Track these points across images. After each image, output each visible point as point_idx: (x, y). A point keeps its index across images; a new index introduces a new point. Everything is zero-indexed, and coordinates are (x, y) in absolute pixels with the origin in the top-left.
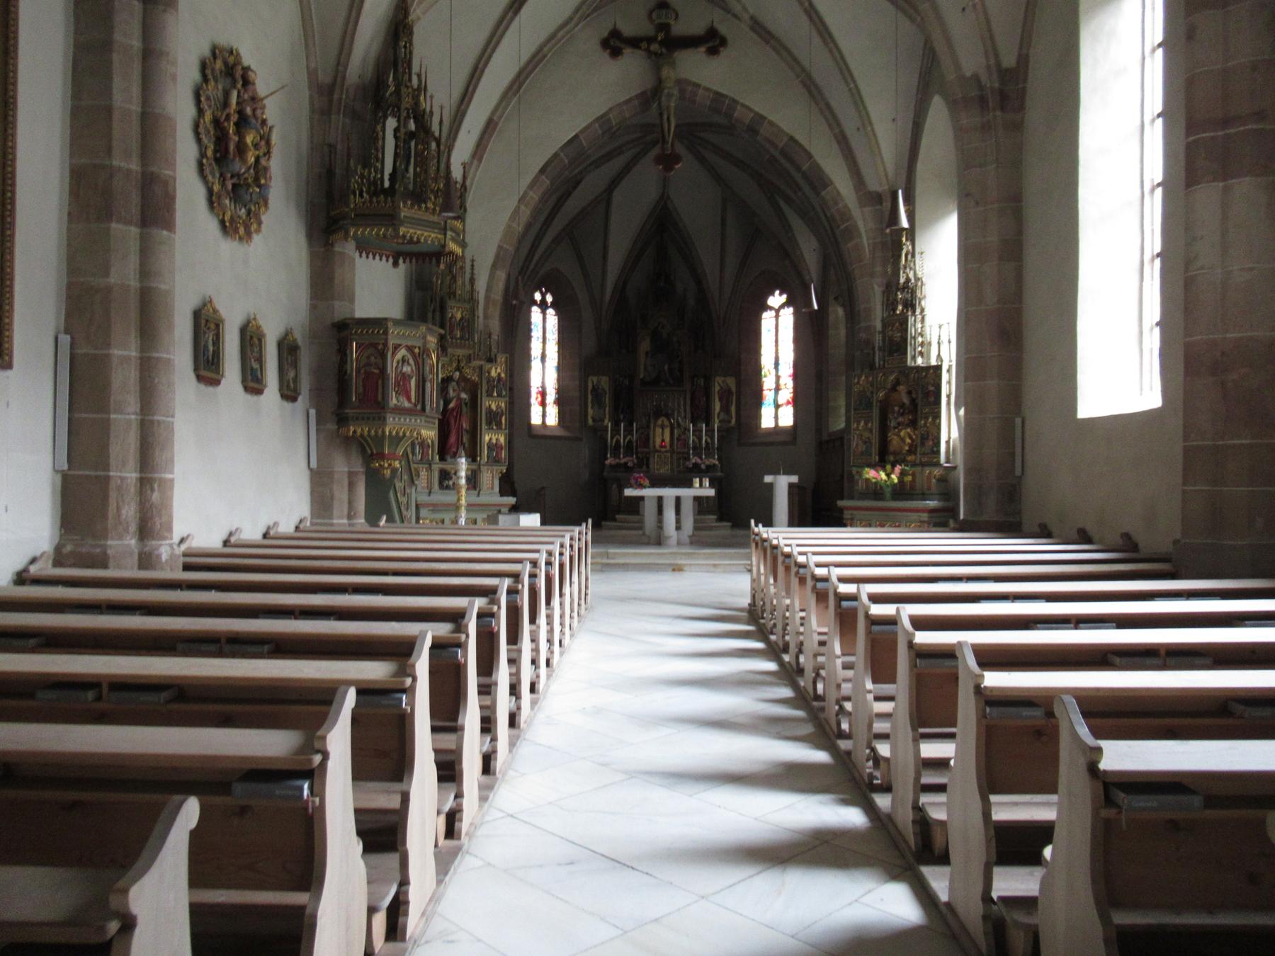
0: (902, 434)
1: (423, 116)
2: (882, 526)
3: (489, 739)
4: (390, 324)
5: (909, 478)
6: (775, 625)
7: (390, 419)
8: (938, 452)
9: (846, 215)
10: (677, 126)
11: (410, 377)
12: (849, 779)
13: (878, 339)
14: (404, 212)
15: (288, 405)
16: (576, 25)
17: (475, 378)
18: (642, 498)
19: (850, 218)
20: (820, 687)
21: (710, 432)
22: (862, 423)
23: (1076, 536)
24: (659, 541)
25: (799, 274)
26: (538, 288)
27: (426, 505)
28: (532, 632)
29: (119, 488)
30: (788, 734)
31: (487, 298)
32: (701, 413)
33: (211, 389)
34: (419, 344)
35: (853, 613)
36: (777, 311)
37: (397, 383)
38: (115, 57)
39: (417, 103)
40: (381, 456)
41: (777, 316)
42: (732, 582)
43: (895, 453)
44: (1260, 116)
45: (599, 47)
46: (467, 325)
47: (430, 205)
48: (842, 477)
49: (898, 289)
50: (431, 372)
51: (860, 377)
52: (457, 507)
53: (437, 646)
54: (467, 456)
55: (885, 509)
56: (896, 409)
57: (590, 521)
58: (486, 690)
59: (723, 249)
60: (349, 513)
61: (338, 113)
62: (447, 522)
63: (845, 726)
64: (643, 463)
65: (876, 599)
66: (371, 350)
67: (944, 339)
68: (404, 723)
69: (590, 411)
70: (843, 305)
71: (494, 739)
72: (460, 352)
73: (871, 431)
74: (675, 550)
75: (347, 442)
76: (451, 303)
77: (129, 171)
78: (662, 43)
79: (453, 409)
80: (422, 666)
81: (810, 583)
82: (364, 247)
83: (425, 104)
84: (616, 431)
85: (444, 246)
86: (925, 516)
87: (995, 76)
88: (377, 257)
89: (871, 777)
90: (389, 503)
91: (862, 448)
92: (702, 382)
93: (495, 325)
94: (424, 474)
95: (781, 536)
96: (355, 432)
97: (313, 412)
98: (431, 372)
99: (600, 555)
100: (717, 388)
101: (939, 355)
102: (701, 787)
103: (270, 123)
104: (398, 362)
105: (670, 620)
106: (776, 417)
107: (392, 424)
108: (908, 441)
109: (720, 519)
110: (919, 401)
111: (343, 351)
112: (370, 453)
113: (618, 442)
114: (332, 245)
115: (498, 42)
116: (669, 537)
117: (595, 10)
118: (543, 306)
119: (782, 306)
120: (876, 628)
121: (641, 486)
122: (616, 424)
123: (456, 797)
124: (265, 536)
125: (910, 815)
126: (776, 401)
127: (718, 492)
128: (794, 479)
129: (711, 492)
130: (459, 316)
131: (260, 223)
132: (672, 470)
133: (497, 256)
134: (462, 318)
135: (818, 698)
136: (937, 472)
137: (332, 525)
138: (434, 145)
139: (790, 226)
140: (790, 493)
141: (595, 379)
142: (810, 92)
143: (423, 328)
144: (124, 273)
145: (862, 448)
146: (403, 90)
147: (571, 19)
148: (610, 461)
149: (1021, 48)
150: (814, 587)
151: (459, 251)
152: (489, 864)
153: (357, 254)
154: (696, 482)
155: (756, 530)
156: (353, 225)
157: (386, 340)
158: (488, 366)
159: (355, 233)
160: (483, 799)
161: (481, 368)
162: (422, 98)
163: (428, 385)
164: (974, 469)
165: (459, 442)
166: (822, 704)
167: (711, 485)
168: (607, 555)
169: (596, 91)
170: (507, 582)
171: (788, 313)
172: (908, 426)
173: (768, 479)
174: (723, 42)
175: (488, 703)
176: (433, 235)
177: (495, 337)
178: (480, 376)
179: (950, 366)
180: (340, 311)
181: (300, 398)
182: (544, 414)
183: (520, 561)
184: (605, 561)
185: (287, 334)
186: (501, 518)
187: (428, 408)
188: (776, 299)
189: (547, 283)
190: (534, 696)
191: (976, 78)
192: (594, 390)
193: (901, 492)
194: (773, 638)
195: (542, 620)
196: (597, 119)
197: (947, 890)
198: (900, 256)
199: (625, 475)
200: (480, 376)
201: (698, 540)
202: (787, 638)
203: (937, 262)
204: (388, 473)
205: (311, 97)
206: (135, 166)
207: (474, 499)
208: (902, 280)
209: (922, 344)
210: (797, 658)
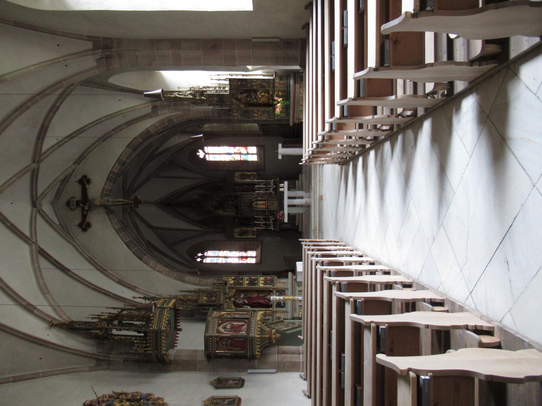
0: (260, 96)
1: (111, 317)
2: (302, 105)
3: (395, 285)
4: (208, 334)
5: (280, 93)
6: (350, 152)
8: (268, 80)
9: (162, 122)
10: (124, 198)
11: (232, 325)
12: (443, 108)
13: (217, 108)
14: (155, 327)
15: (246, 383)
16: (76, 243)
17: (234, 291)
18: (289, 214)
19: (163, 120)
20: (384, 128)
21: (259, 183)
22: (255, 115)
23: (308, 10)
25: (190, 144)
26: (195, 259)
27: (293, 314)
28: (347, 265)
30: (412, 143)
31: (197, 285)
32: (251, 187)
33: (242, 402)
34: (216, 321)
35: (350, 108)
36: (206, 154)
37: (235, 331)
39: (105, 320)
40: (270, 338)
41: (208, 154)
42: (328, 173)
43: (269, 100)
46: (210, 294)
47: (152, 315)
48: (279, 125)
49: (195, 99)
50: (230, 314)
51: (234, 116)
52: (294, 300)
53: (340, 290)
54: (270, 294)
55: (294, 104)
56: (249, 99)
57: (300, 240)
58: (360, 274)
60: (297, 353)
61: (109, 357)
62: (300, 304)
63: (409, 113)
64: (273, 213)
65: (332, 114)
66: (220, 344)
67: (217, 77)
68: (393, 327)
69: (250, 236)
70: (203, 124)
71: (396, 283)
72: (222, 297)
73: (258, 111)
74: (312, 199)
75: (263, 354)
76: (200, 302)
78: (85, 205)
79: (248, 301)
80: (366, 319)
81: (333, 134)
82: (172, 345)
83: (106, 316)
84: (259, 225)
85: (171, 309)
86: (298, 86)
87: (97, 51)
88: (177, 338)
89: (443, 95)
91: (266, 115)
93: (210, 281)
94: (278, 315)
95: (307, 150)
96: (258, 352)
97: (249, 371)
98: (230, 314)
99: (315, 233)
100: (240, 180)
101: (224, 80)
102: (448, 188)
103: (111, 393)
104: (225, 331)
105: (347, 203)
106: (253, 154)
107: (255, 333)
108: (263, 94)
109: (298, 179)
110: (245, 89)
111: (220, 357)
112: (268, 344)
113: (263, 224)
114: (171, 361)
115: (84, 280)
116: (307, 202)
117: (70, 235)
118: (203, 257)
119: (204, 152)
120: (362, 94)
121: (283, 214)
122: (255, 225)
123: (425, 301)
124: (309, 397)
125: (476, 67)
126: (245, 154)
127: (286, 180)
128: (280, 145)
129: (286, 183)
130: (205, 298)
131: (159, 398)
133: (179, 280)
134: (207, 297)
135: (392, 128)
136: (277, 80)
137: (303, 362)
138: (125, 312)
140: (287, 147)
141: (235, 234)
142: (107, 138)
143: (209, 318)
145: (266, 115)
146: (99, 326)
148: (272, 228)
149: (84, 39)
150: (335, 131)
151: (173, 301)
152: (510, 311)
153: (176, 348)
154: (281, 190)
155: (304, 162)
156: (161, 352)
157: (215, 336)
158: (228, 285)
159: (164, 351)
160: (461, 309)
161: (229, 288)
162: (103, 317)
163: (236, 316)
164: (277, 61)
165: (263, 298)
166: (395, 126)
167: (283, 183)
168: (315, 230)
169: (104, 233)
170: (319, 266)
172: (256, 94)
173: (280, 157)
174: (85, 177)
175: (379, 286)
176: (165, 314)
177: (215, 281)
179: (230, 75)
180: (201, 357)
181: (243, 377)
182: (251, 257)
183: (316, 270)
184: (318, 231)
185: (212, 384)
186: (298, 280)
187: (247, 316)
188: (201, 154)
189: (193, 256)
190: (392, 273)
191: (97, 60)
192: (240, 235)
193: (286, 97)
194: (357, 153)
195: (341, 259)
196: (118, 234)
197: (531, 38)
198: (180, 98)
199: (278, 222)
200: (233, 288)
201: (308, 189)
202: (357, 146)
203: (183, 80)
204: (278, 335)
205: (103, 370)
207: (290, 292)
208: (191, 97)
209: (220, 88)
210: (368, 140)
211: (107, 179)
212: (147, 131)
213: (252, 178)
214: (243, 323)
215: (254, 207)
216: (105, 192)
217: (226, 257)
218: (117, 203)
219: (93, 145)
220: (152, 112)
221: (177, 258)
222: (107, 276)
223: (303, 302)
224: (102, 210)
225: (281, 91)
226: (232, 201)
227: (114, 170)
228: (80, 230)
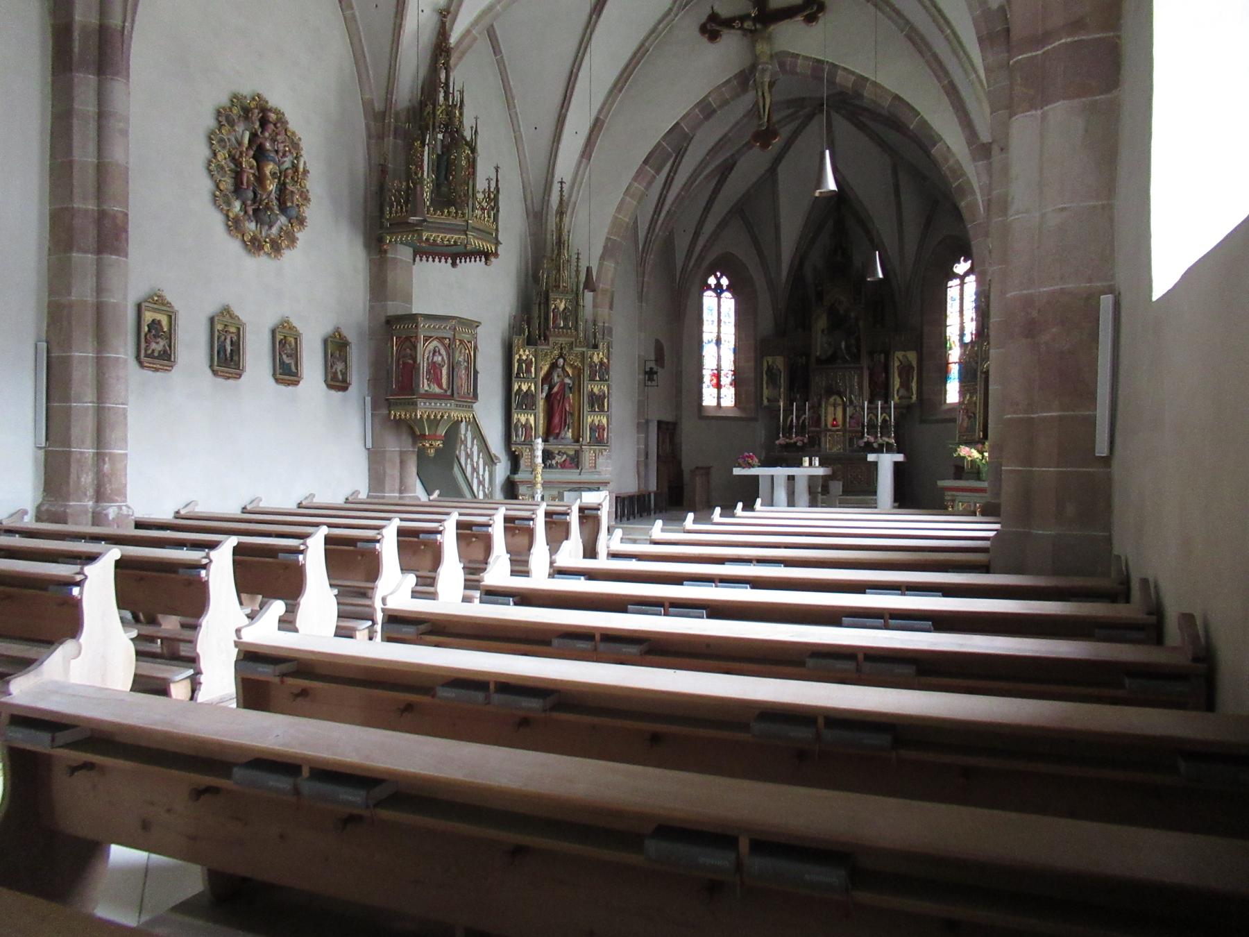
7: (421, 404)
9: (958, 172)
17: (578, 364)
19: (963, 174)
21: (885, 409)
29: (79, 461)
32: (880, 391)
34: (450, 334)
36: (962, 278)
38: (75, 121)
44: (1077, 25)
45: (697, 33)
69: (766, 392)
72: (562, 340)
75: (398, 423)
76: (552, 296)
77: (86, 211)
78: (755, 20)
79: (557, 393)
84: (788, 411)
90: (454, 479)
97: (368, 399)
100: (897, 364)
114: (386, 252)
118: (718, 290)
119: (967, 274)
122: (790, 403)
128: (900, 457)
130: (562, 306)
132: (845, 450)
133: (605, 247)
137: (383, 497)
141: (770, 359)
144: (82, 291)
147: (671, 9)
154: (806, 460)
173: (871, 457)
180: (394, 308)
182: (719, 395)
188: (962, 267)
189: (724, 265)
192: (769, 369)
200: (583, 361)
206: (91, 206)
212: (935, 139)
213: (902, 392)
214: (445, 386)
216: (789, 60)
221: (709, 228)
222: (611, 92)
223: (530, 501)
226: (847, 347)
227: (840, 72)
228: (704, 18)
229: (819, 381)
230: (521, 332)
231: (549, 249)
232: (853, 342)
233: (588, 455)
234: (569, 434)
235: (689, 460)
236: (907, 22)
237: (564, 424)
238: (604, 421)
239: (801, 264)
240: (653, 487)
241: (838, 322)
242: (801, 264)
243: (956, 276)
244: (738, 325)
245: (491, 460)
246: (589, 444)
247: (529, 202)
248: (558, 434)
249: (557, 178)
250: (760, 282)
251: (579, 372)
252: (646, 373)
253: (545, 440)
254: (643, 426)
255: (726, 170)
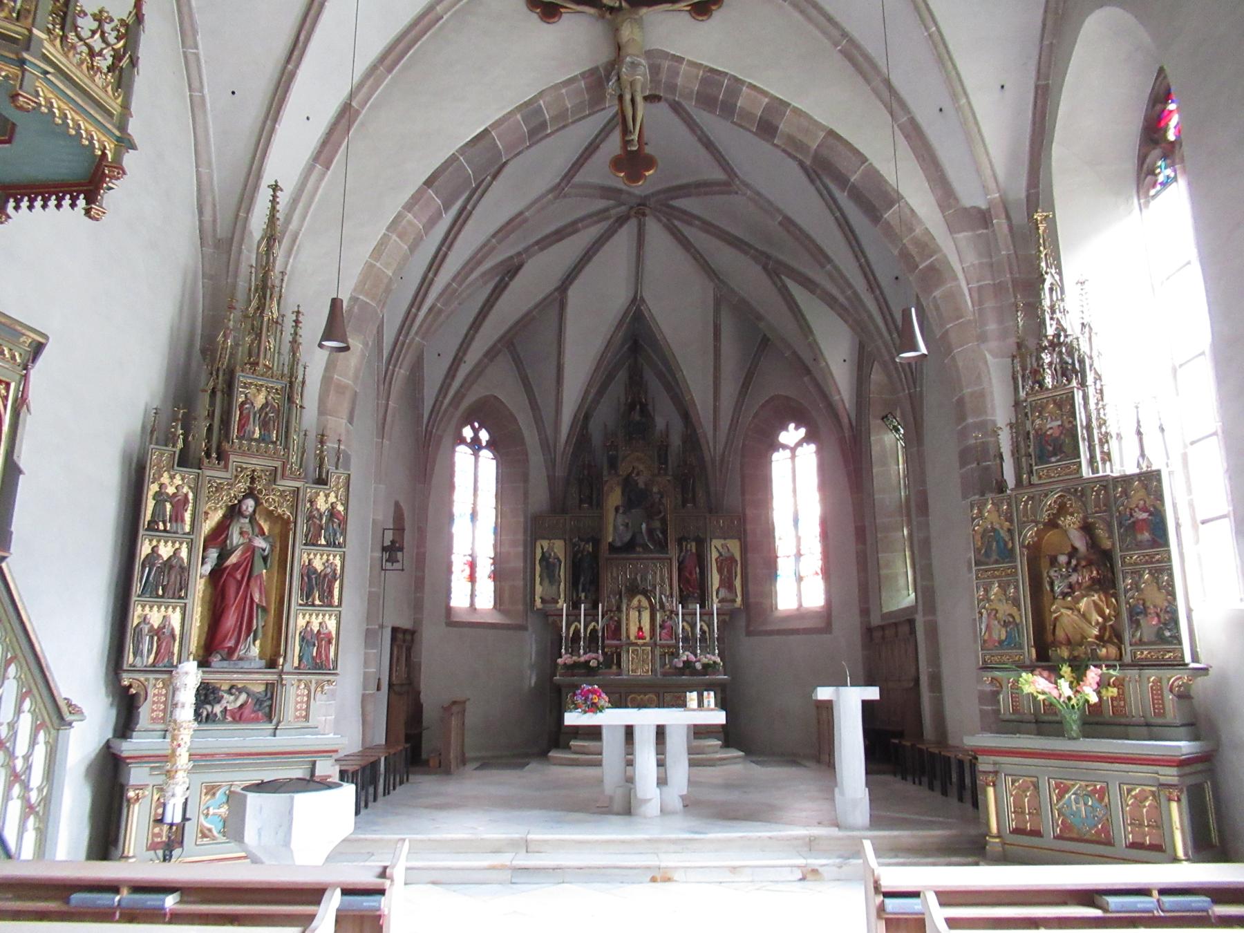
0: (1082, 605)
5: (1113, 691)
9: (927, 246)
19: (937, 250)
21: (707, 615)
22: (995, 588)
24: (627, 808)
26: (468, 421)
32: (693, 589)
36: (793, 450)
41: (793, 457)
59: (717, 368)
64: (612, 660)
72: (257, 463)
76: (242, 377)
79: (236, 566)
84: (574, 616)
86: (1170, 775)
92: (693, 547)
100: (715, 555)
113: (577, 631)
116: (646, 801)
118: (475, 445)
119: (799, 444)
121: (595, 708)
122: (575, 605)
128: (873, 693)
129: (720, 718)
130: (260, 400)
136: (1174, 677)
139: (809, 327)
141: (545, 544)
148: (565, 659)
154: (692, 697)
167: (722, 704)
171: (809, 451)
173: (824, 693)
178: (295, 508)
182: (472, 591)
184: (523, 860)
188: (791, 435)
189: (484, 413)
192: (544, 558)
196: (519, 108)
200: (295, 508)
208: (1050, 331)
211: (712, 70)
212: (892, 198)
213: (723, 593)
215: (630, 600)
216: (666, 64)
217: (474, 516)
218: (628, 97)
219: (830, 19)
220: (966, 210)
222: (373, 68)
224: (603, 56)
225: (1121, 696)
226: (650, 532)
229: (614, 577)
230: (169, 440)
231: (241, 295)
232: (657, 524)
233: (292, 695)
234: (255, 650)
235: (433, 693)
236: (845, 34)
237: (246, 629)
238: (331, 625)
239: (587, 417)
240: (381, 739)
241: (635, 498)
242: (587, 417)
243: (784, 447)
244: (500, 496)
245: (57, 715)
246: (298, 670)
247: (208, 217)
248: (231, 651)
249: (267, 180)
250: (531, 437)
251: (284, 528)
252: (384, 549)
253: (203, 663)
254: (370, 637)
255: (511, 270)
